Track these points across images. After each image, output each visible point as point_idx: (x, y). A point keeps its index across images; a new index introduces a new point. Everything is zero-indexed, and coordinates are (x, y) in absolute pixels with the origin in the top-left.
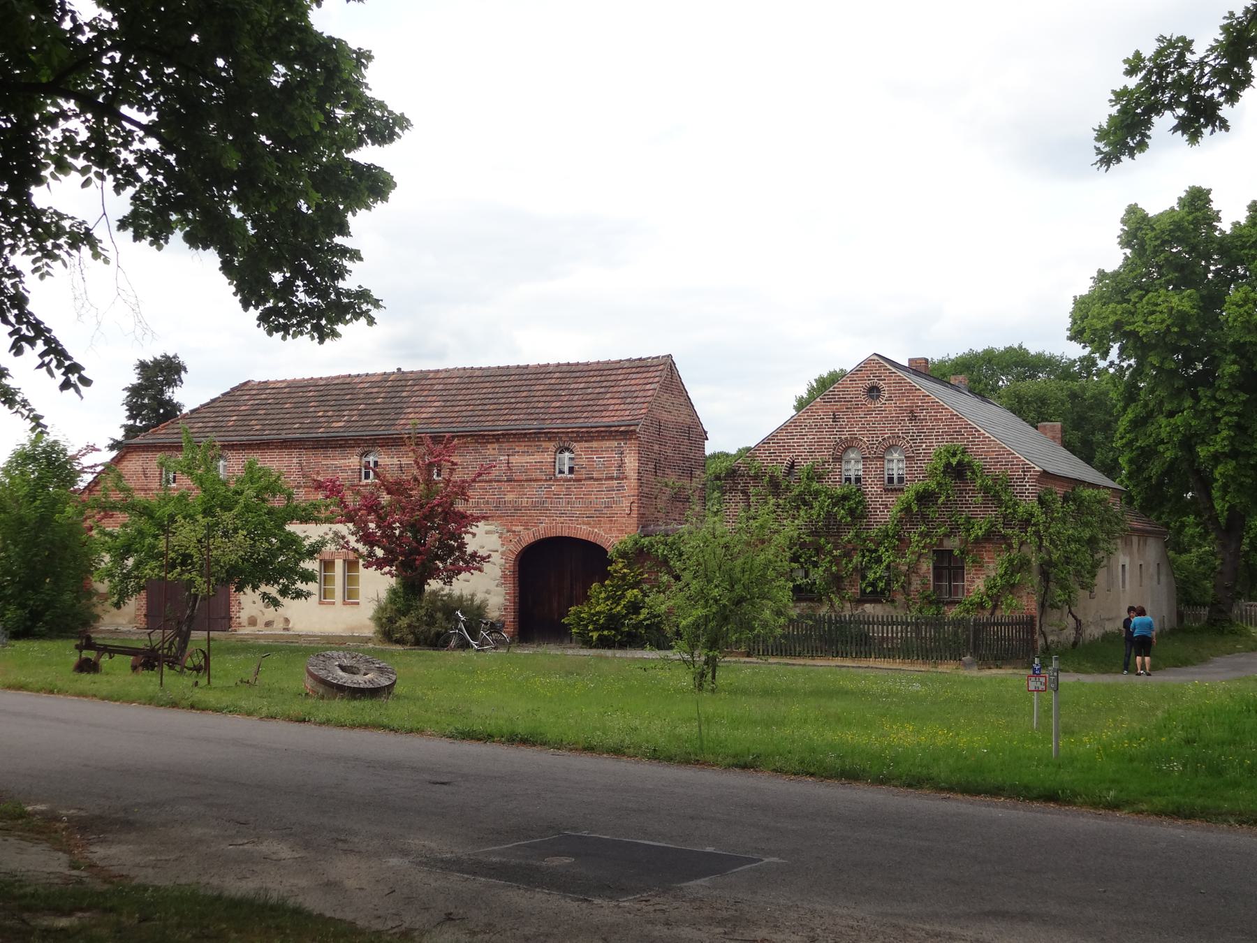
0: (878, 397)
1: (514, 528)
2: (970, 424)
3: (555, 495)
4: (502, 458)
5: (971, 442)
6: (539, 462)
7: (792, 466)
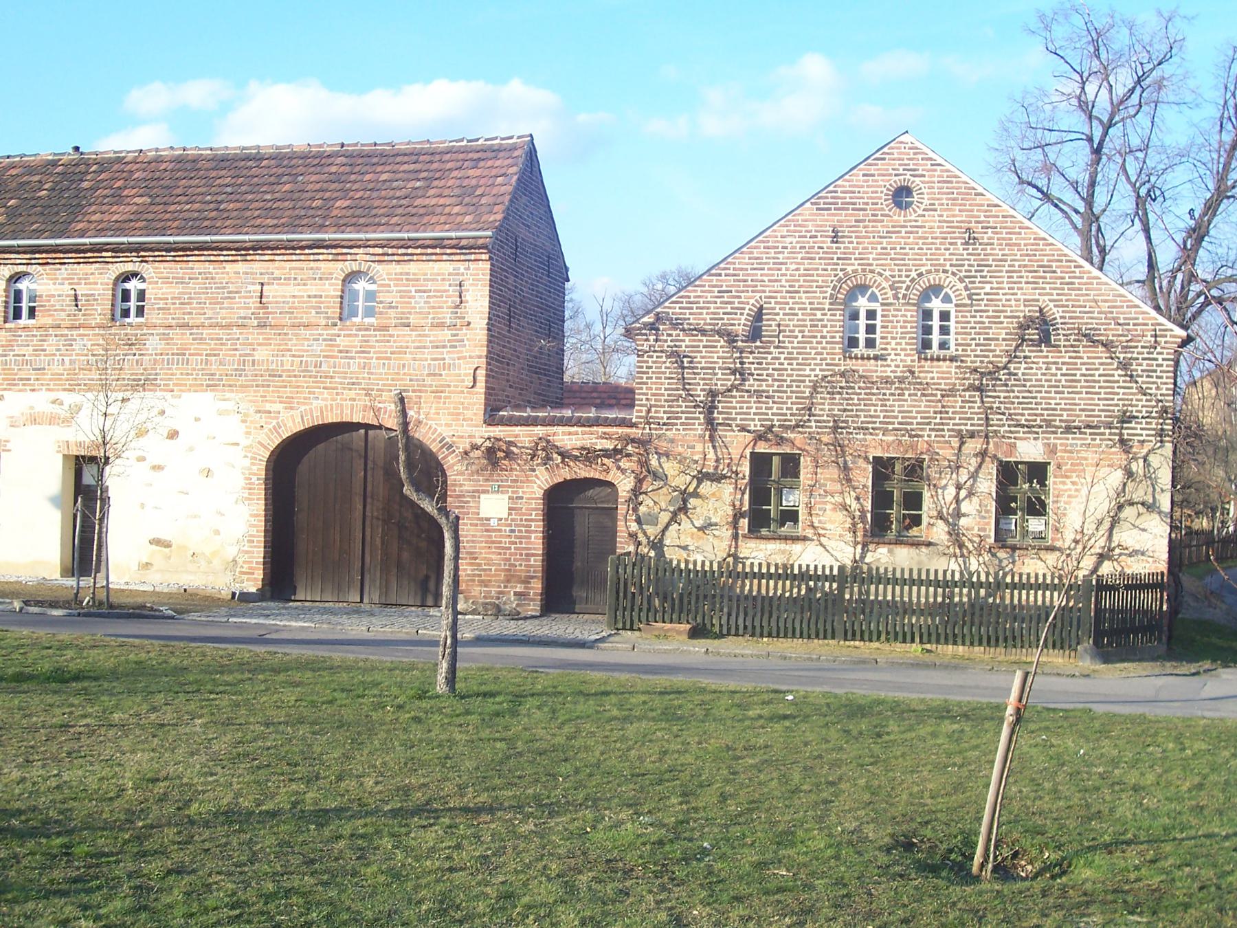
0: (909, 205)
1: (268, 407)
2: (1065, 255)
3: (341, 352)
4: (251, 288)
5: (1068, 284)
6: (315, 296)
7: (759, 315)
